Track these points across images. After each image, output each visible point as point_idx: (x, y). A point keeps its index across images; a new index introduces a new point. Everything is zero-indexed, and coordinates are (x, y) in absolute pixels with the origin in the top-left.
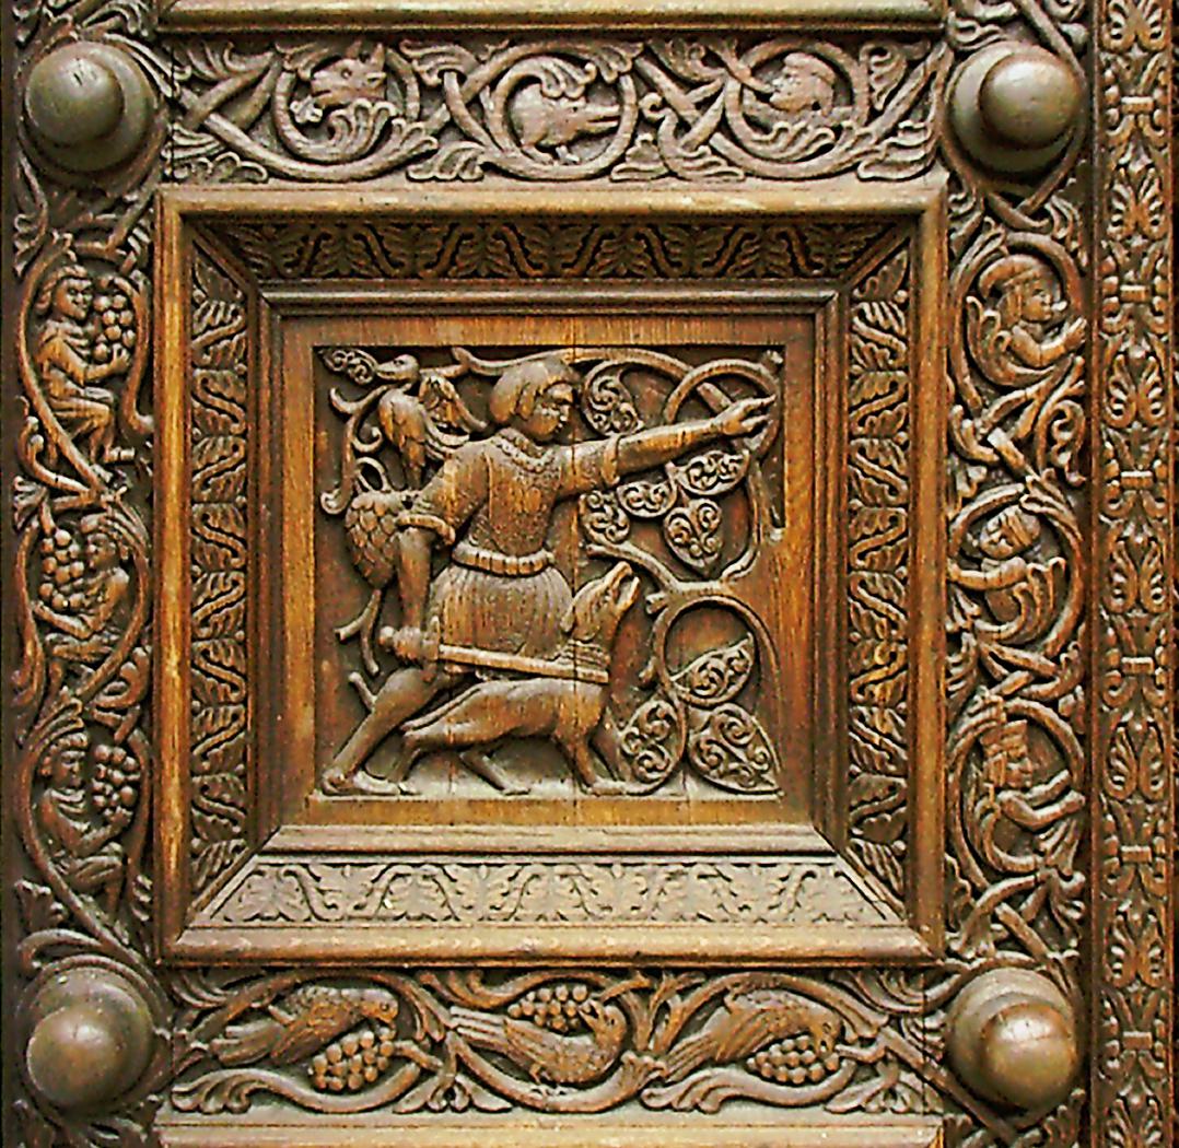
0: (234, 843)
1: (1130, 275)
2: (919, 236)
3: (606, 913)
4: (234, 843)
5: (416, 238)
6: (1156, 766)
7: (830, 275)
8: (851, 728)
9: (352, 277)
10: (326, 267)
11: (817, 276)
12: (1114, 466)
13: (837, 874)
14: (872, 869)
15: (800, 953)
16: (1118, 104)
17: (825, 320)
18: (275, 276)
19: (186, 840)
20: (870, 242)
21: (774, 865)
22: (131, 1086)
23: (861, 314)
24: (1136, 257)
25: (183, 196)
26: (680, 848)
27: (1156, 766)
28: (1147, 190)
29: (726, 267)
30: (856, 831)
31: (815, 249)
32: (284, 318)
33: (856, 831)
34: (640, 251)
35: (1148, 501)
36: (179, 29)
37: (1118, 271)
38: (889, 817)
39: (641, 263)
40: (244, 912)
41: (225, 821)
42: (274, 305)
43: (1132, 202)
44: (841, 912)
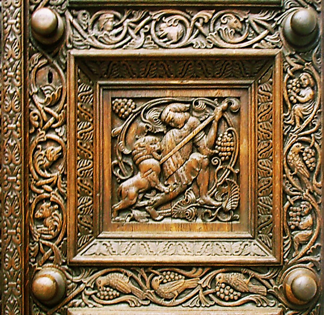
0: (89, 235)
1: (10, 69)
2: (275, 64)
3: (228, 253)
4: (89, 235)
5: (138, 65)
6: (17, 208)
7: (251, 77)
8: (258, 204)
9: (123, 77)
10: (152, 75)
11: (248, 77)
12: (6, 123)
13: (254, 245)
14: (263, 242)
15: (172, 261)
16: (7, 179)
17: (251, 89)
18: (102, 78)
19: (76, 234)
20: (263, 66)
21: (161, 242)
22: (59, 298)
23: (261, 88)
24: (12, 65)
25: (74, 52)
26: (205, 237)
27: (17, 208)
28: (14, 46)
29: (184, 75)
30: (260, 232)
31: (247, 69)
32: (103, 90)
33: (260, 232)
34: (124, 69)
35: (15, 133)
36: (100, 5)
37: (7, 69)
38: (267, 227)
39: (125, 73)
40: (94, 252)
41: (86, 228)
42: (101, 86)
43: (10, 49)
44: (255, 252)
